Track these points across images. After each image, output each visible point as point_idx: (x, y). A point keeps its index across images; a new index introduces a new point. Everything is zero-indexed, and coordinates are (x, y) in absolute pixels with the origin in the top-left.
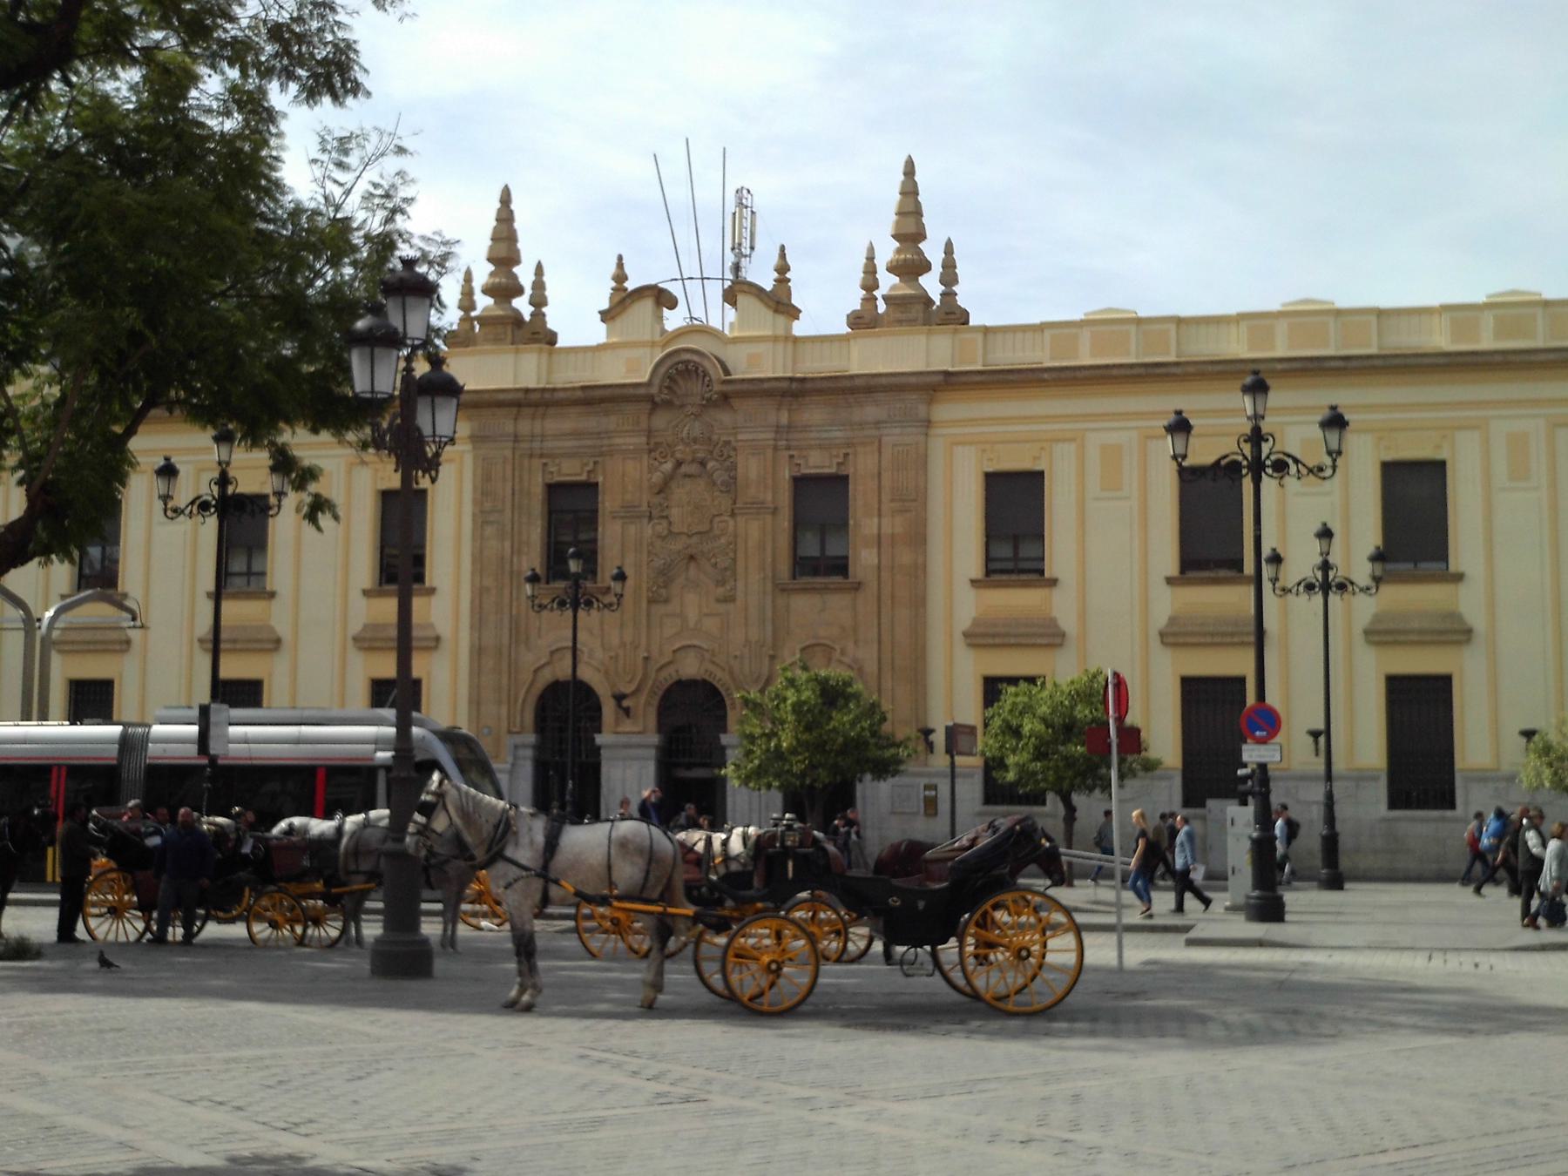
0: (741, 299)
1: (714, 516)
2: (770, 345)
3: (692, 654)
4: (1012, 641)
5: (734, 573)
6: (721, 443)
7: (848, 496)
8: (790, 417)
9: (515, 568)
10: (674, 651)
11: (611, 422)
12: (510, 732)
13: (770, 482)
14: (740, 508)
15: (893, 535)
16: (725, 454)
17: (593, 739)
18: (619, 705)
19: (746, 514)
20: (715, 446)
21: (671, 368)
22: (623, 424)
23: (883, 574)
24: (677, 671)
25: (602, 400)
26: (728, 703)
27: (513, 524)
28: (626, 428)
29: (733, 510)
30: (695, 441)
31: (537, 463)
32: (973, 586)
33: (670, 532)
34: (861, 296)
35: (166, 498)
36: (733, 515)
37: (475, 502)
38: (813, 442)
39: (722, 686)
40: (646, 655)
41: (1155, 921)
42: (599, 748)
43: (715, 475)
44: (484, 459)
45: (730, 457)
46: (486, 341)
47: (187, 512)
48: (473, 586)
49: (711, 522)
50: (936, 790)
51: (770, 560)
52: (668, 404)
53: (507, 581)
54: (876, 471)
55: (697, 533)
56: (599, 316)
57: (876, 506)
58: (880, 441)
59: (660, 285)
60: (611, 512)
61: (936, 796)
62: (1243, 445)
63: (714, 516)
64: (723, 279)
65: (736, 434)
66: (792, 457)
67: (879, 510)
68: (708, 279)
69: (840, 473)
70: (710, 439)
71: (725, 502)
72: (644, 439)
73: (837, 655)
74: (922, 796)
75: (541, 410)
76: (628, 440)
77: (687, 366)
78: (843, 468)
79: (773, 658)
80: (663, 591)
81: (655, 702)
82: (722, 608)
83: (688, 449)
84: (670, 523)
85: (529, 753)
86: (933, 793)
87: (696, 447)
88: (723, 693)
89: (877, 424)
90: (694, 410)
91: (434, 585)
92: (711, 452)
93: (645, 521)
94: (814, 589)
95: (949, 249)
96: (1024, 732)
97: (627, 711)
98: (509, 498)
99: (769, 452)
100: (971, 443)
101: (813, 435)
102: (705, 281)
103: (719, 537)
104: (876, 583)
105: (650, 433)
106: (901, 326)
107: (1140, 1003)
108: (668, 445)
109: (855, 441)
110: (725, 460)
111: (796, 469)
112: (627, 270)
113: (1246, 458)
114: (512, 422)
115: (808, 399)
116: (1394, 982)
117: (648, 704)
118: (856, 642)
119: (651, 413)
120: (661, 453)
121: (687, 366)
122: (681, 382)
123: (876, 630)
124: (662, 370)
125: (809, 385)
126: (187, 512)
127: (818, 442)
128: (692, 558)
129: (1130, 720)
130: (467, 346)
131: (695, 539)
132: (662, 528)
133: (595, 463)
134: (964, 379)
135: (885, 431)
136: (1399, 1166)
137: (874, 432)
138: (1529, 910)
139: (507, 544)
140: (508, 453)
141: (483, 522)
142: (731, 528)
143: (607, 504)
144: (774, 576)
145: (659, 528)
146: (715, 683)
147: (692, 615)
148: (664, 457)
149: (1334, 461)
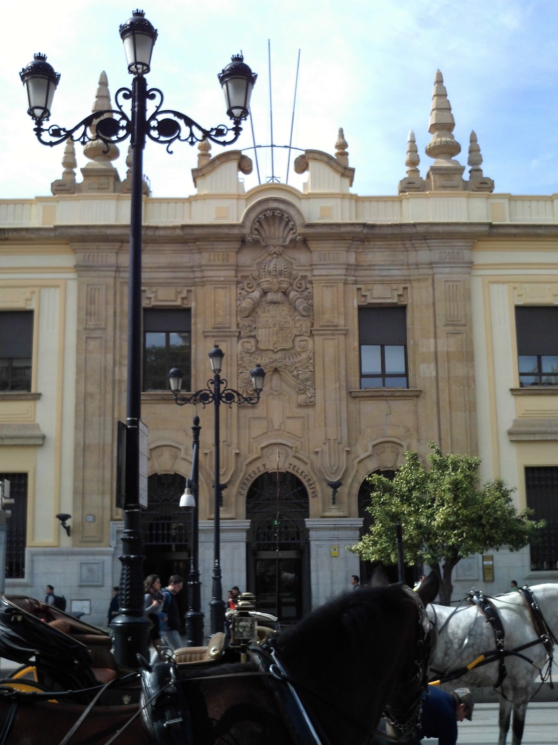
1: (296, 336)
2: (339, 201)
3: (277, 450)
4: (549, 438)
6: (299, 278)
8: (356, 259)
9: (117, 378)
10: (262, 448)
11: (204, 258)
12: (112, 519)
13: (342, 309)
14: (316, 330)
16: (304, 286)
19: (324, 335)
20: (294, 279)
21: (260, 214)
23: (440, 384)
24: (264, 465)
25: (196, 240)
26: (309, 491)
27: (115, 341)
28: (217, 263)
29: (311, 331)
32: (513, 394)
33: (257, 348)
36: (312, 335)
37: (79, 321)
38: (376, 278)
39: (304, 478)
40: (238, 451)
42: (308, 530)
43: (297, 303)
44: (88, 285)
45: (307, 289)
46: (91, 189)
48: (77, 392)
49: (293, 341)
50: (492, 560)
52: (256, 243)
53: (109, 388)
54: (431, 301)
57: (432, 330)
58: (433, 280)
61: (493, 565)
62: (210, 385)
63: (296, 336)
65: (312, 270)
66: (359, 289)
68: (260, 146)
69: (400, 303)
70: (291, 274)
71: (305, 325)
72: (233, 273)
74: (481, 565)
75: (408, 244)
76: (222, 273)
77: (273, 213)
79: (348, 452)
82: (303, 412)
83: (275, 280)
84: (257, 342)
86: (491, 563)
87: (282, 279)
88: (306, 484)
89: (431, 264)
90: (276, 250)
91: (39, 391)
92: (291, 284)
94: (382, 396)
95: (473, 139)
98: (111, 319)
99: (341, 285)
100: (503, 283)
101: (376, 273)
102: (288, 145)
103: (299, 354)
105: (237, 268)
106: (446, 190)
107: (13, 634)
108: (253, 278)
109: (411, 278)
110: (303, 291)
111: (363, 299)
113: (211, 392)
114: (115, 254)
115: (372, 243)
117: (240, 494)
118: (418, 440)
120: (249, 284)
121: (273, 213)
123: (436, 427)
124: (253, 215)
125: (377, 231)
127: (380, 278)
130: (73, 193)
131: (279, 355)
132: (251, 345)
133: (189, 291)
134: (502, 231)
137: (430, 272)
139: (110, 357)
140: (111, 281)
141: (87, 338)
143: (199, 326)
144: (347, 386)
145: (248, 346)
148: (250, 288)
149: (237, 122)
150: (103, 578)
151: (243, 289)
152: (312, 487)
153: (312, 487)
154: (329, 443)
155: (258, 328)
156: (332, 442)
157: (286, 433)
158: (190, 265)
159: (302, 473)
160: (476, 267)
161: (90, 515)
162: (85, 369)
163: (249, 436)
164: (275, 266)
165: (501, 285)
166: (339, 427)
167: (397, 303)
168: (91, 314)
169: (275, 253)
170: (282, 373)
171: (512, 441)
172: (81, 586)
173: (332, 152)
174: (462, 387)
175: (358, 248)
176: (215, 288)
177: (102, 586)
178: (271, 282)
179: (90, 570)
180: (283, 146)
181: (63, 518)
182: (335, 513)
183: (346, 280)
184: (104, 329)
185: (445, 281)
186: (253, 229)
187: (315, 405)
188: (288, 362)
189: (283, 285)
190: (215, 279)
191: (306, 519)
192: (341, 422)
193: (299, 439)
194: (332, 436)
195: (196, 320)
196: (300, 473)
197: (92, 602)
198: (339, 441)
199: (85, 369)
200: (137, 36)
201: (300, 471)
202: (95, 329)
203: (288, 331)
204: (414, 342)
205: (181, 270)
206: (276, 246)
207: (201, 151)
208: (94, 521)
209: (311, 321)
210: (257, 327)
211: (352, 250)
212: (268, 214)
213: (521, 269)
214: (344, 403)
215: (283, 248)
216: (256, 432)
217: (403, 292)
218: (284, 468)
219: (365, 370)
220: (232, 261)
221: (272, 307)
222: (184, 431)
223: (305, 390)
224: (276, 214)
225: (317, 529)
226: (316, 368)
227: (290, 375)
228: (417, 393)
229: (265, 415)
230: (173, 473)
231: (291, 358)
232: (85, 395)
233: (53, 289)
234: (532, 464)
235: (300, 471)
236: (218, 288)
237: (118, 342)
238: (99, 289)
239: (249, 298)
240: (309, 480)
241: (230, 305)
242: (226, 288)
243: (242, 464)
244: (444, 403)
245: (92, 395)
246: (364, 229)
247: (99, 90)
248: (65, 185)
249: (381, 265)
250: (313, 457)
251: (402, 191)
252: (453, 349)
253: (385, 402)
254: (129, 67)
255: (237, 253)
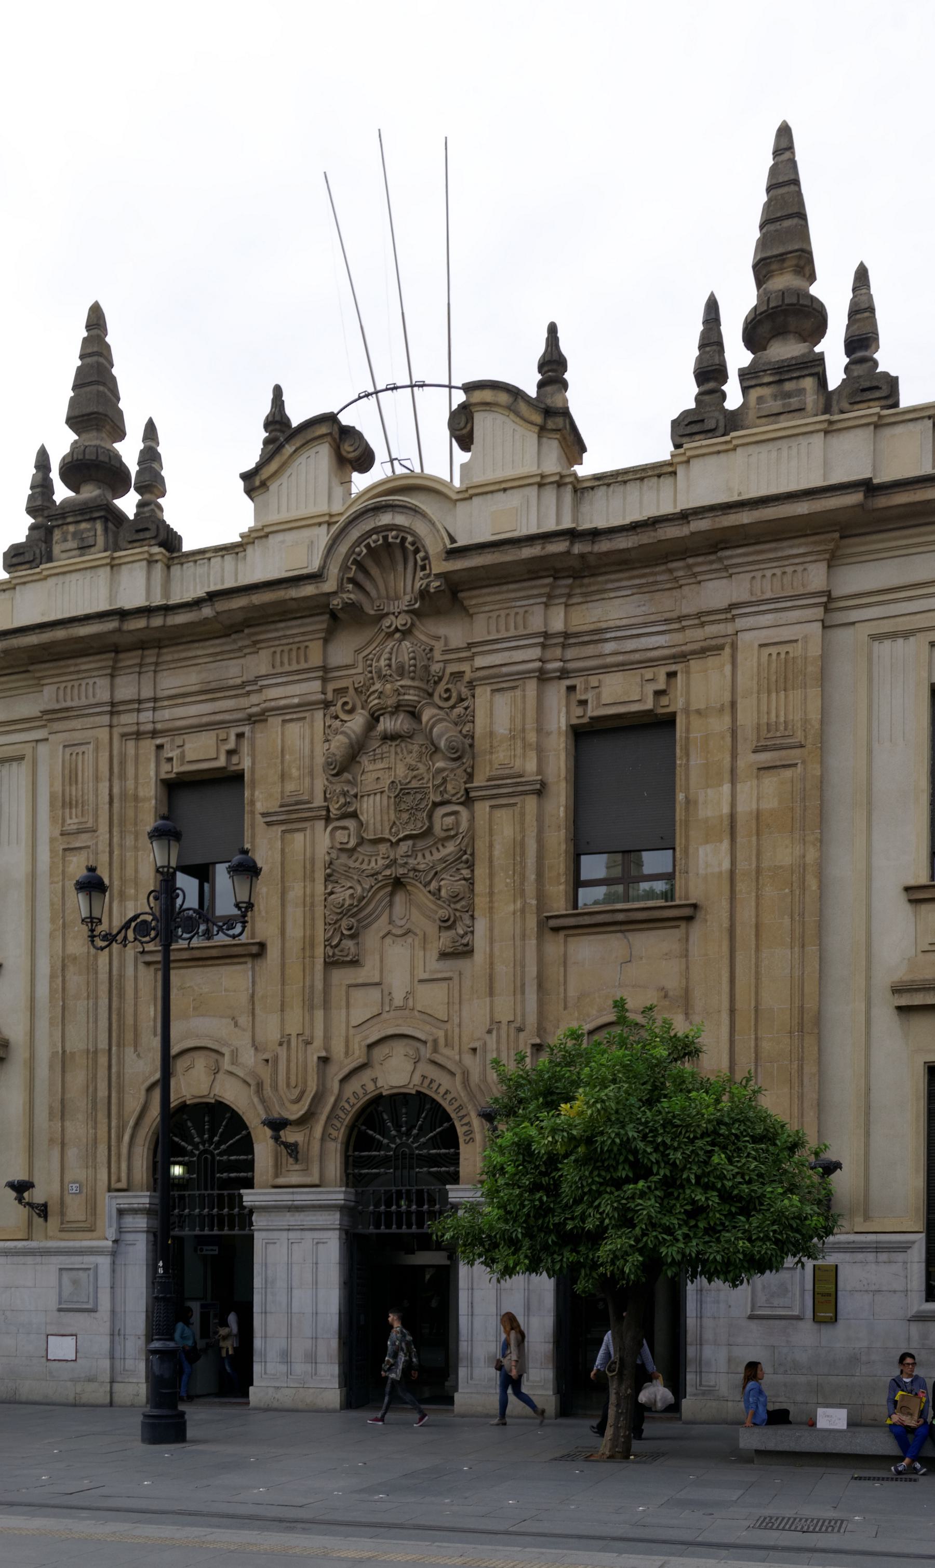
0: (483, 423)
1: (436, 805)
3: (399, 1049)
5: (470, 910)
7: (675, 740)
10: (370, 1046)
13: (532, 737)
15: (758, 815)
17: (241, 1196)
18: (276, 1138)
20: (436, 683)
21: (358, 543)
22: (282, 663)
24: (375, 1080)
26: (460, 1130)
27: (111, 853)
29: (467, 791)
30: (401, 671)
31: (148, 746)
34: (136, 501)
35: (92, 921)
40: (323, 1054)
41: (579, 911)
44: (65, 746)
47: (120, 938)
49: (430, 816)
51: (533, 877)
54: (727, 697)
55: (406, 838)
56: (241, 484)
59: (454, 407)
60: (264, 815)
63: (436, 805)
64: (450, 387)
65: (471, 658)
67: (733, 771)
68: (423, 385)
70: (426, 668)
72: (316, 685)
73: (226, 1064)
75: (151, 656)
77: (385, 538)
78: (664, 701)
80: (349, 944)
81: (340, 1134)
85: (141, 1222)
87: (406, 682)
90: (400, 622)
93: (320, 824)
96: (126, 623)
97: (293, 1150)
101: (609, 647)
104: (725, 904)
110: (453, 707)
112: (565, 347)
116: (566, 808)
119: (328, 638)
120: (345, 703)
121: (385, 538)
122: (374, 571)
126: (120, 938)
128: (398, 884)
129: (269, 719)
132: (347, 836)
133: (240, 736)
135: (741, 623)
136: (695, 428)
138: (169, 1103)
140: (103, 734)
142: (464, 825)
144: (540, 908)
145: (341, 836)
146: (438, 1098)
147: (398, 984)
150: (96, 1298)
151: (336, 717)
152: (465, 1121)
153: (465, 1121)
154: (498, 1029)
155: (362, 796)
156: (504, 1027)
157: (416, 1013)
158: (238, 681)
159: (446, 1093)
160: (159, 568)
161: (74, 1183)
162: (64, 911)
163: (348, 1022)
164: (387, 662)
165: (900, 641)
166: (519, 997)
167: (651, 711)
168: (112, 713)
169: (397, 630)
170: (409, 888)
171: (900, 1009)
172: (60, 1310)
173: (529, 382)
174: (787, 891)
175: (569, 596)
176: (284, 721)
177: (94, 1310)
178: (381, 693)
179: (75, 1282)
180: (857, 625)
181: (21, 1188)
182: (294, 1179)
183: (541, 671)
184: (94, 831)
185: (761, 646)
186: (345, 580)
187: (472, 951)
188: (421, 862)
189: (407, 697)
190: (282, 702)
191: (448, 1187)
192: (523, 985)
193: (442, 1025)
194: (293, 1028)
195: (253, 795)
196: (441, 1094)
197: (49, 1333)
198: (518, 1025)
199: (64, 911)
200: (93, 894)
201: (442, 1090)
202: (80, 832)
203: (419, 796)
204: (686, 798)
205: (227, 694)
206: (399, 613)
207: (34, 517)
208: (80, 1192)
209: (465, 771)
210: (359, 794)
211: (557, 601)
212: (374, 542)
213: (910, 599)
214: (533, 942)
215: (414, 618)
216: (359, 1014)
217: (668, 683)
218: (411, 1086)
219: (671, 851)
220: (315, 659)
221: (389, 748)
222: (233, 1018)
223: (454, 922)
224: (390, 540)
225: (265, 1209)
226: (476, 872)
227: (425, 891)
228: (687, 912)
229: (377, 980)
230: (213, 1101)
231: (434, 850)
232: (63, 960)
233: (15, 764)
234: (926, 708)
235: (442, 1090)
236: (291, 720)
237: (116, 853)
238: (83, 753)
239: (342, 733)
240: (460, 1108)
241: (312, 757)
242: (305, 718)
243: (332, 1079)
244: (746, 933)
245: (75, 959)
246: (572, 543)
247: (773, 171)
248: (23, 553)
249: (619, 628)
250: (468, 1060)
251: (677, 446)
252: (770, 803)
253: (619, 935)
254: (912, 1356)
255: (326, 641)
